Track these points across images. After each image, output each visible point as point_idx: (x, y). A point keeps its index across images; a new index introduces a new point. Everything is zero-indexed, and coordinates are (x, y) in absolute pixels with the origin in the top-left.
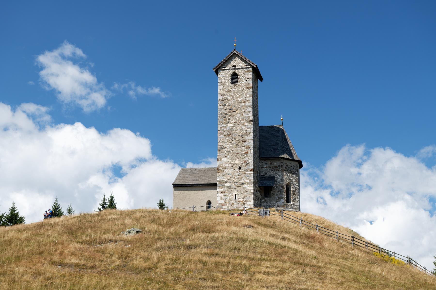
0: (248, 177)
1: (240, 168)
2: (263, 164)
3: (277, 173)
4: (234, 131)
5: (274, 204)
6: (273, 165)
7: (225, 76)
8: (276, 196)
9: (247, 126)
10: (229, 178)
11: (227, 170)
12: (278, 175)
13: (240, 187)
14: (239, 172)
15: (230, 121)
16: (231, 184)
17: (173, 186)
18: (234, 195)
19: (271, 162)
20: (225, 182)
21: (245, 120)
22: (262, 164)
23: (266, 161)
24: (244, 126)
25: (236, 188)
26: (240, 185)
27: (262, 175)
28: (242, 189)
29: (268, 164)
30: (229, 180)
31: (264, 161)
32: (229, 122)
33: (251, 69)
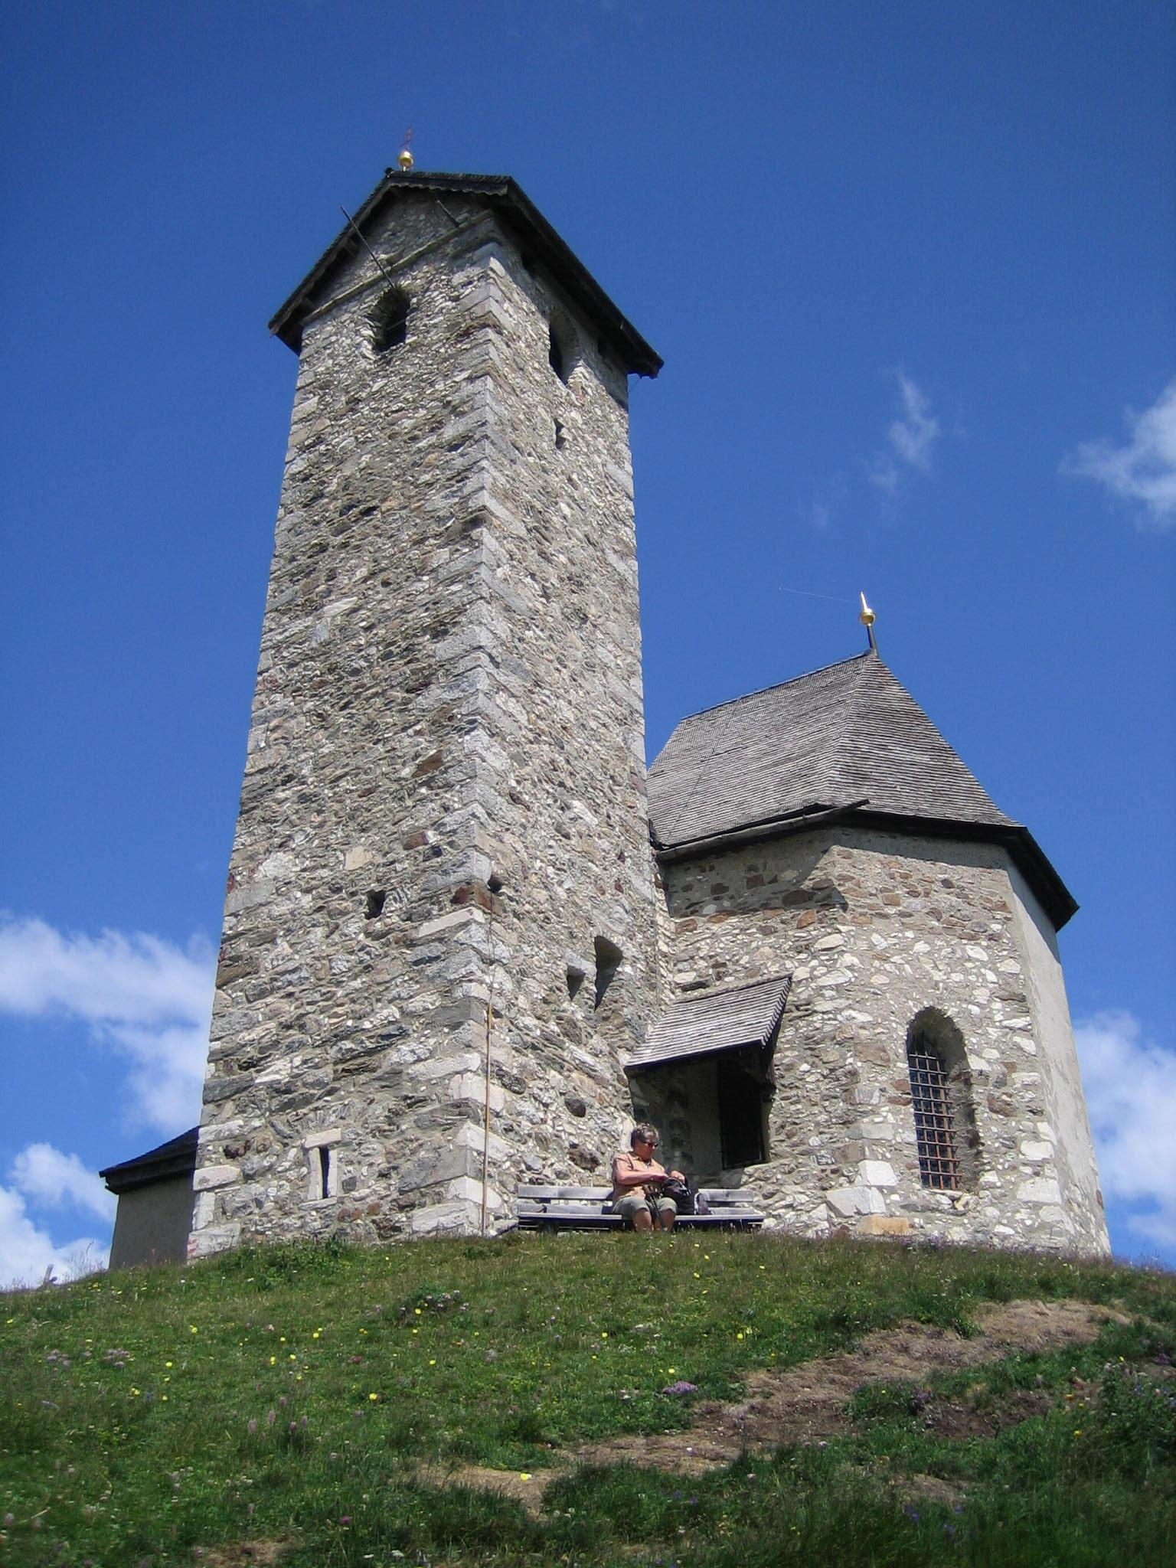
0: (431, 969)
1: (376, 902)
2: (695, 895)
3: (807, 947)
4: (354, 637)
5: (804, 1217)
6: (775, 887)
7: (333, 339)
8: (814, 1141)
9: (443, 573)
10: (289, 1009)
11: (283, 947)
12: (815, 963)
13: (363, 1078)
14: (368, 942)
15: (343, 580)
16: (297, 1061)
17: (103, 1182)
18: (315, 1156)
19: (751, 868)
20: (262, 1050)
21: (435, 537)
22: (688, 894)
23: (712, 868)
24: (425, 578)
25: (337, 1085)
26: (370, 1052)
27: (685, 988)
28: (377, 1084)
29: (730, 893)
30: (288, 1027)
31: (703, 871)
32: (329, 592)
33: (487, 226)
